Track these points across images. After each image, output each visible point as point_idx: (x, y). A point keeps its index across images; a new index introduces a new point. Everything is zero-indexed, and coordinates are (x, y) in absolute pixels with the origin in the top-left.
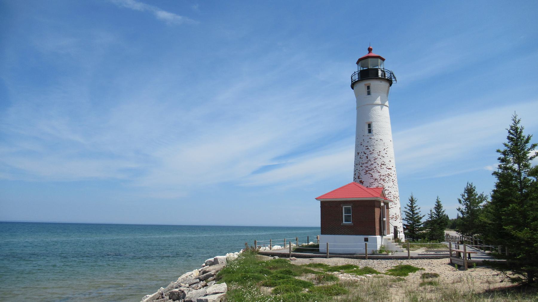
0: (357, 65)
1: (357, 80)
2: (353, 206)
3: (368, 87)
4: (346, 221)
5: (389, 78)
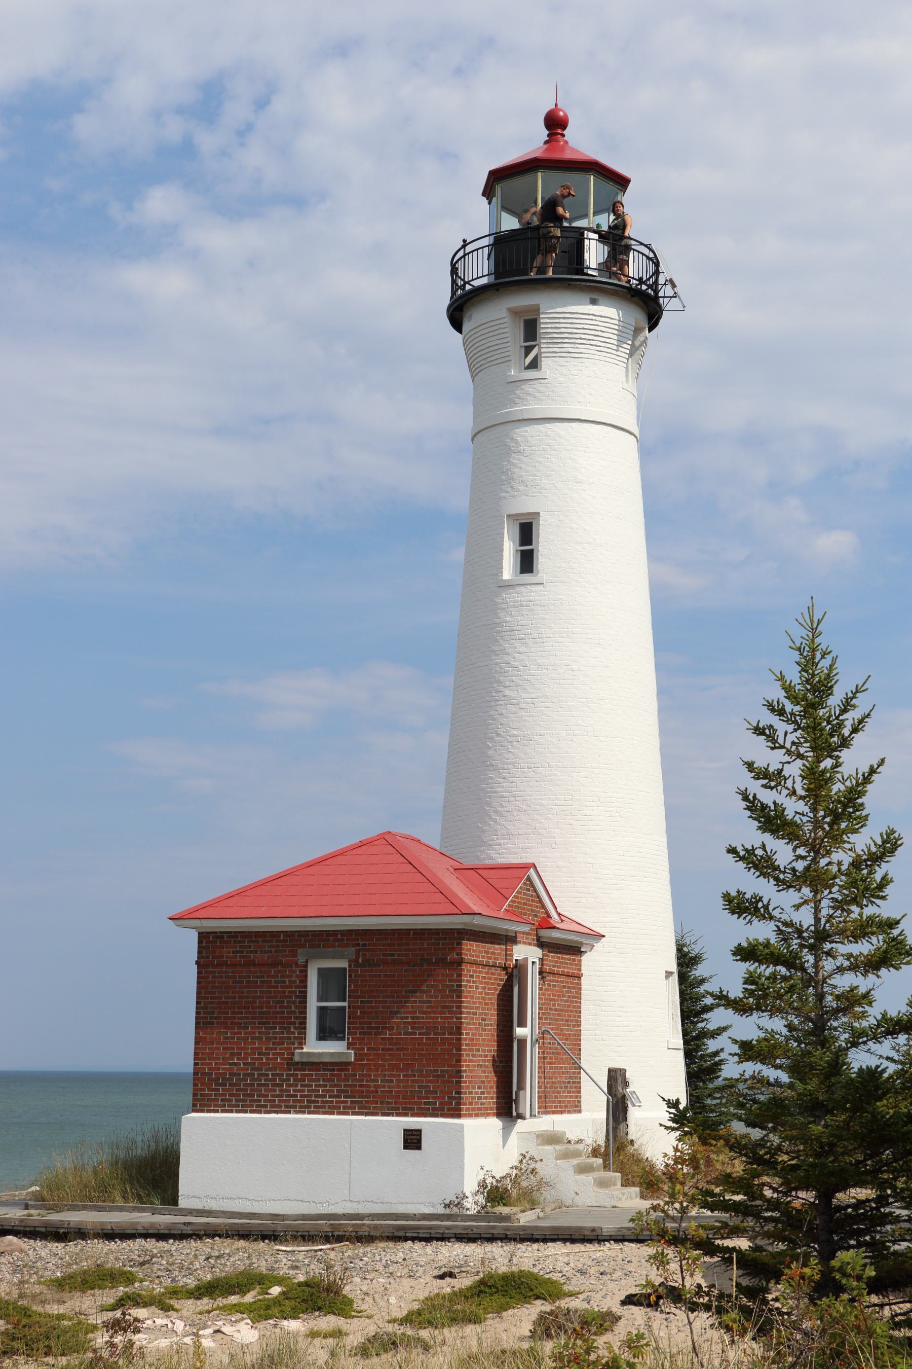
0: (485, 201)
1: (484, 281)
2: (356, 960)
3: (531, 329)
4: (324, 1034)
5: (650, 286)
